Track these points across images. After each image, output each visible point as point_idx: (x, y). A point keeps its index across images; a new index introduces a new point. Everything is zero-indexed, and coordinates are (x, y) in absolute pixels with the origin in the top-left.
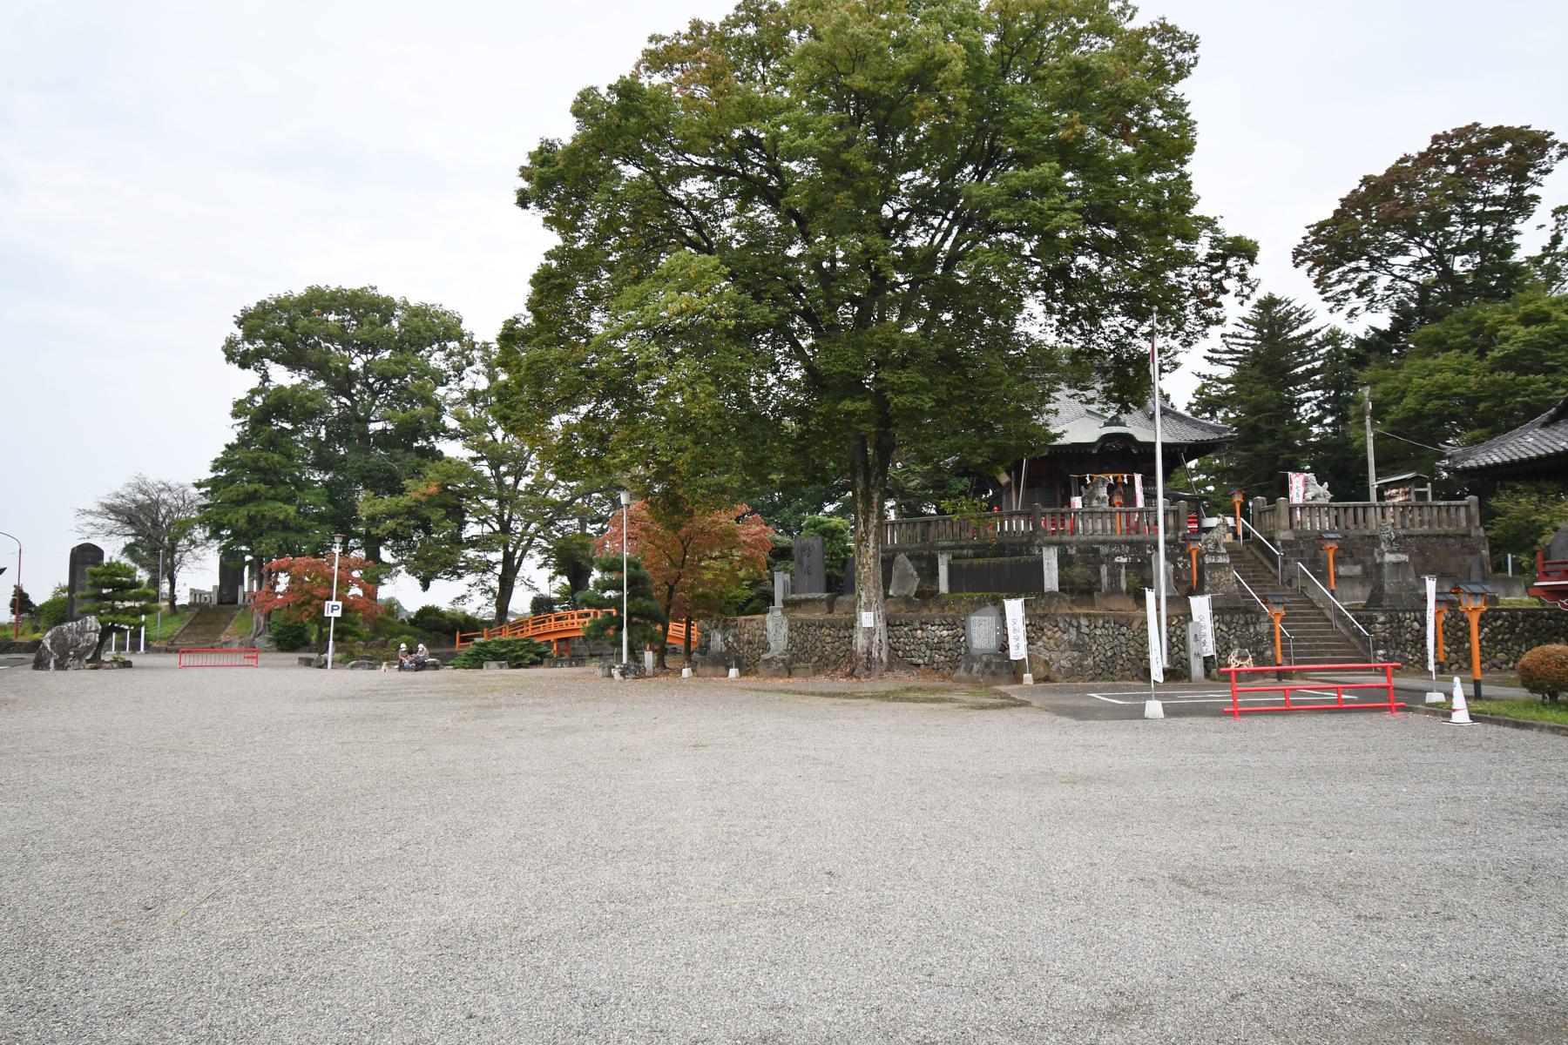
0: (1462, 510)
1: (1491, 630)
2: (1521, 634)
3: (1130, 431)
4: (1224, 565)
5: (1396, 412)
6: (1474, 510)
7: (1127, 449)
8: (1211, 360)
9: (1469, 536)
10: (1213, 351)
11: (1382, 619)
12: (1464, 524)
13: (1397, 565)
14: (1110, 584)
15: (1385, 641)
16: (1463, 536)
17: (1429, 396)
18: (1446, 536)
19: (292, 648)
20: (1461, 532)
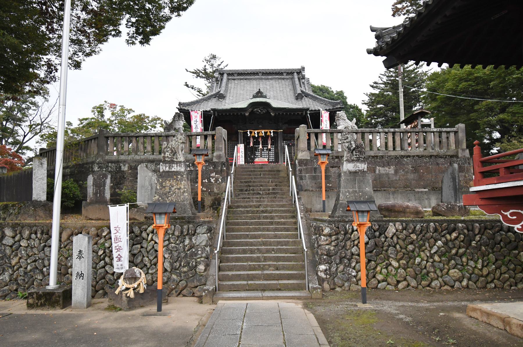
0: (452, 135)
1: (446, 243)
2: (478, 248)
3: (268, 101)
4: (177, 173)
5: (442, 94)
6: (462, 135)
7: (268, 113)
8: (372, 86)
9: (457, 156)
10: (375, 83)
11: (327, 231)
12: (453, 147)
13: (354, 174)
14: (95, 194)
15: (329, 255)
16: (452, 156)
17: (461, 80)
18: (437, 156)
19: (223, 244)
20: (450, 153)
